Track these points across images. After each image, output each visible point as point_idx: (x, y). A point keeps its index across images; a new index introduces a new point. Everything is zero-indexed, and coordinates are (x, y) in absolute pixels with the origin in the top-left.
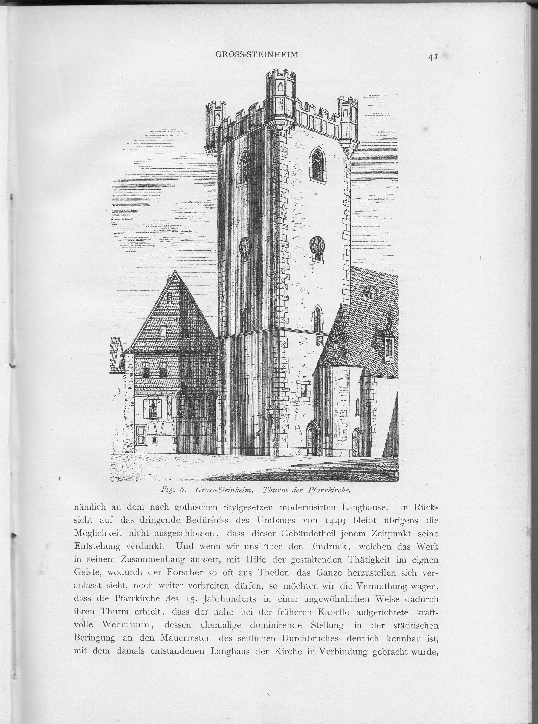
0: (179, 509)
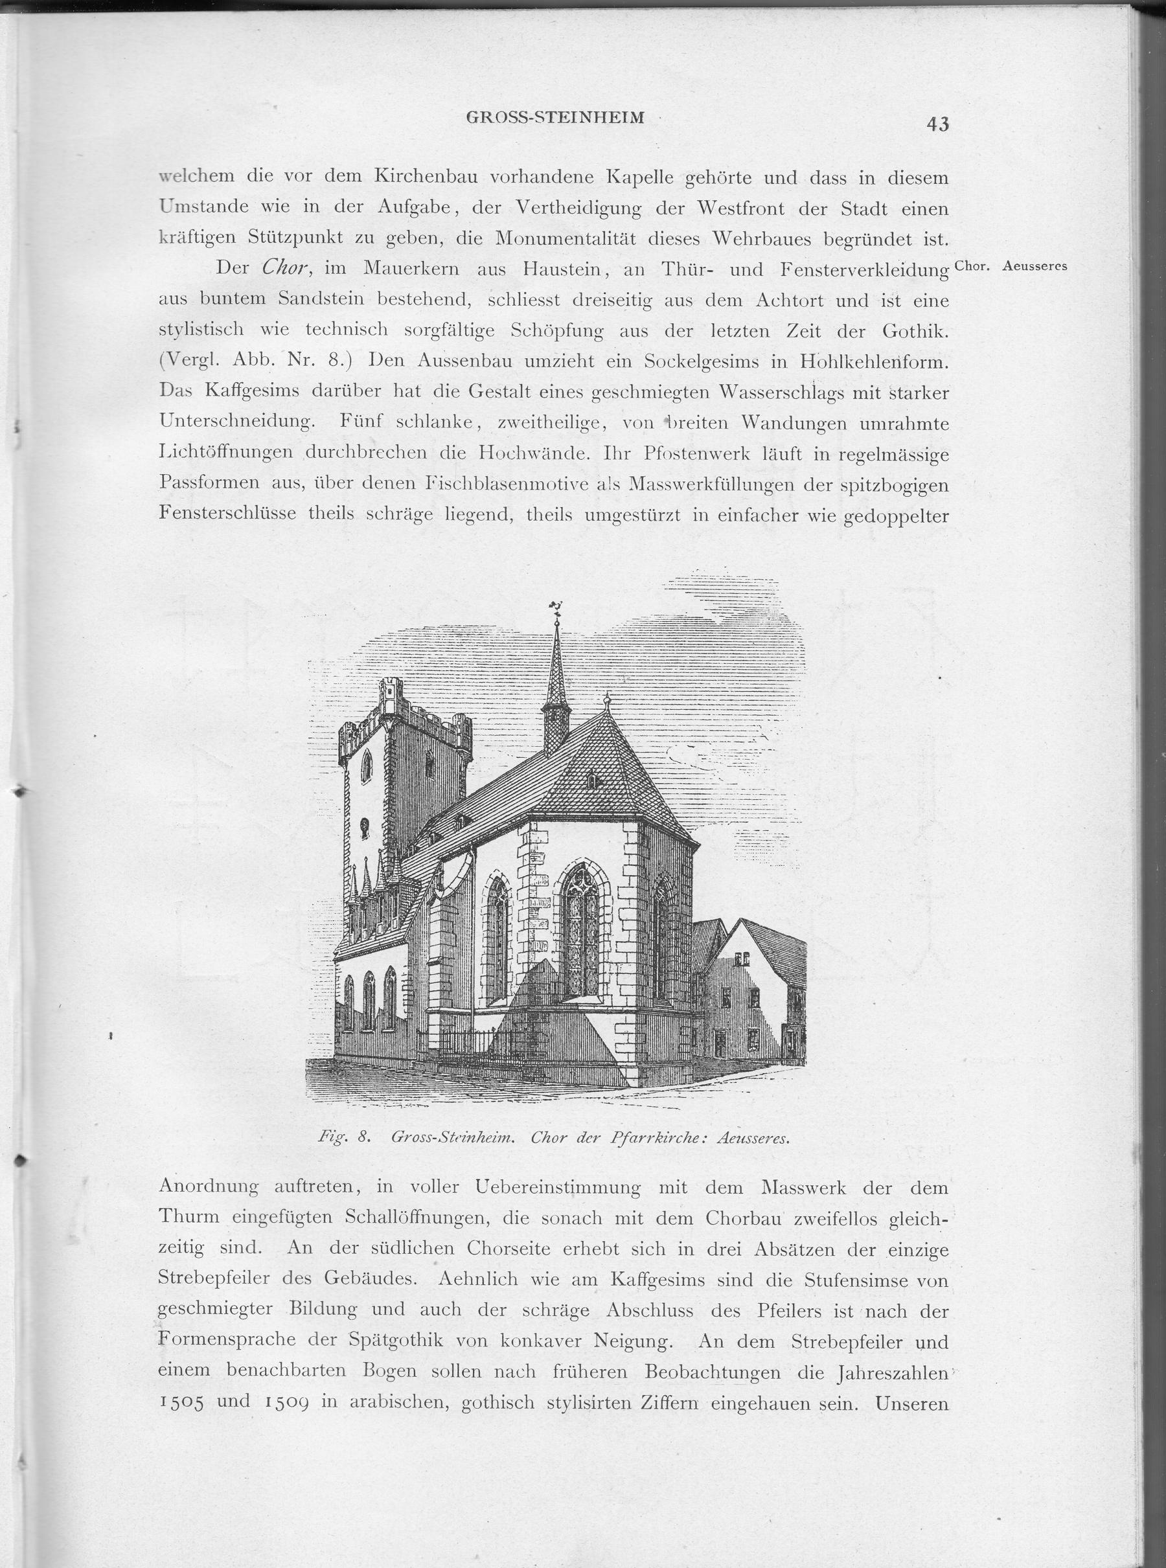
0: (397, 1343)
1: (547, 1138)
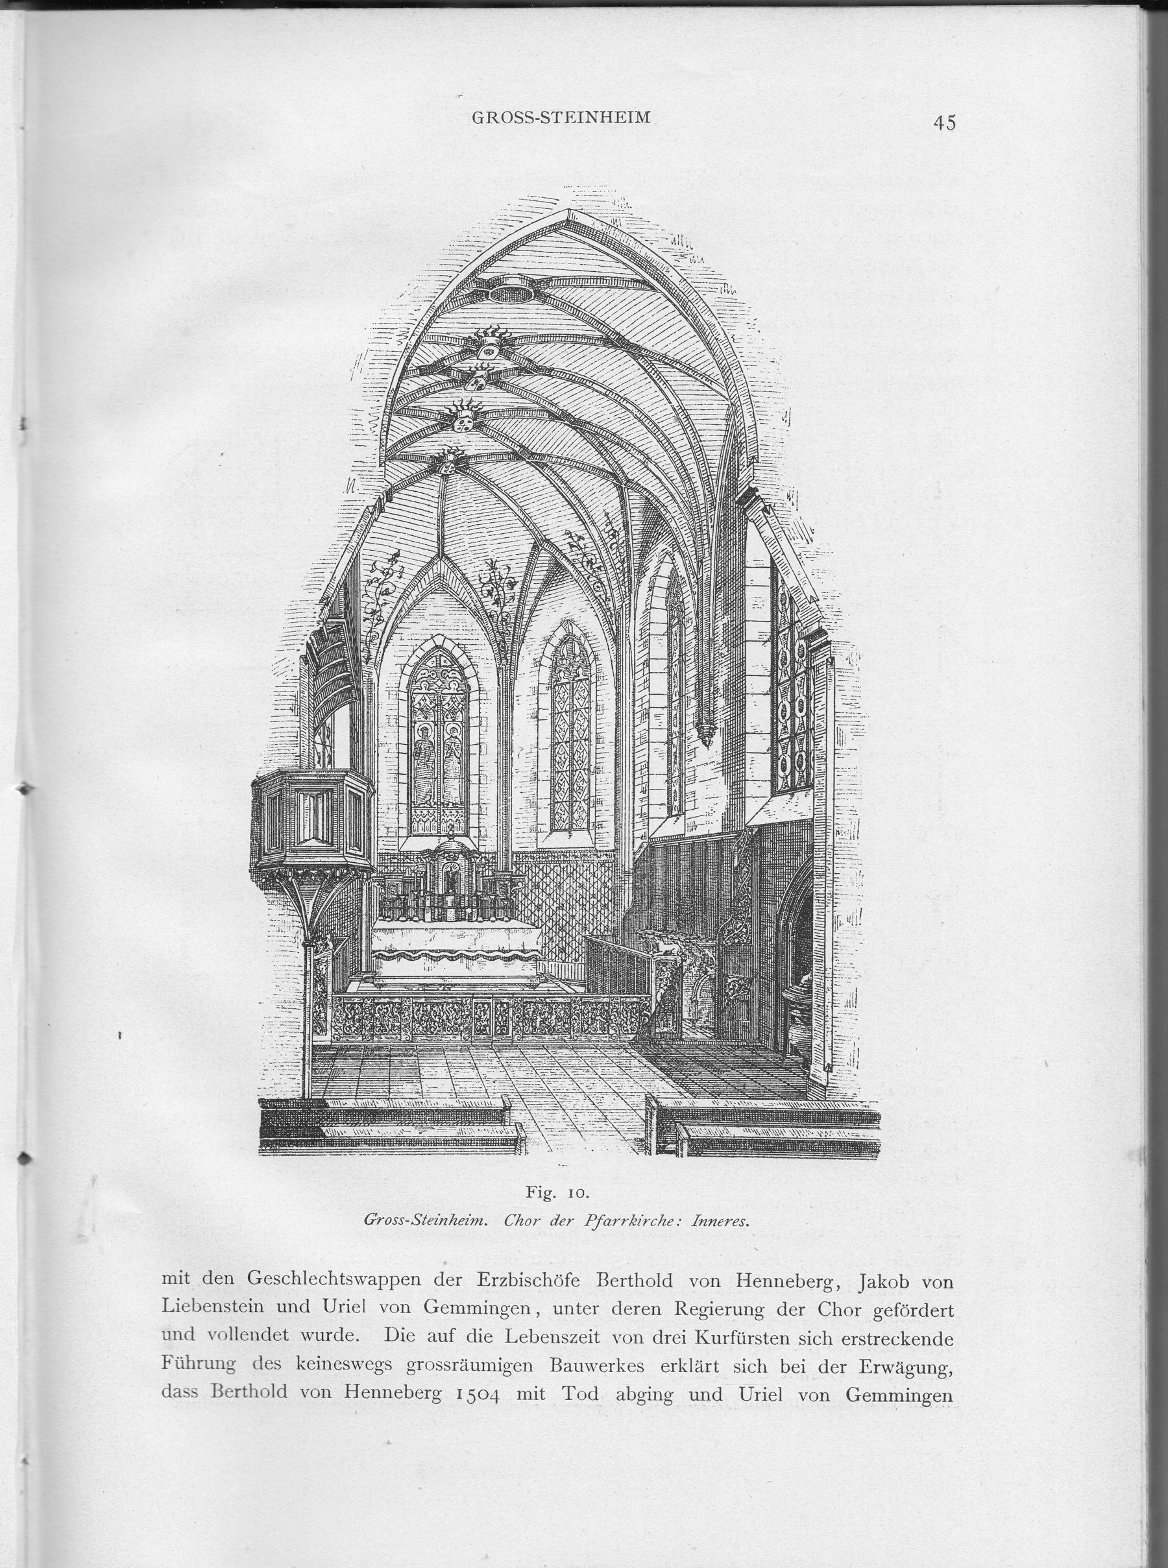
1: (520, 1221)
